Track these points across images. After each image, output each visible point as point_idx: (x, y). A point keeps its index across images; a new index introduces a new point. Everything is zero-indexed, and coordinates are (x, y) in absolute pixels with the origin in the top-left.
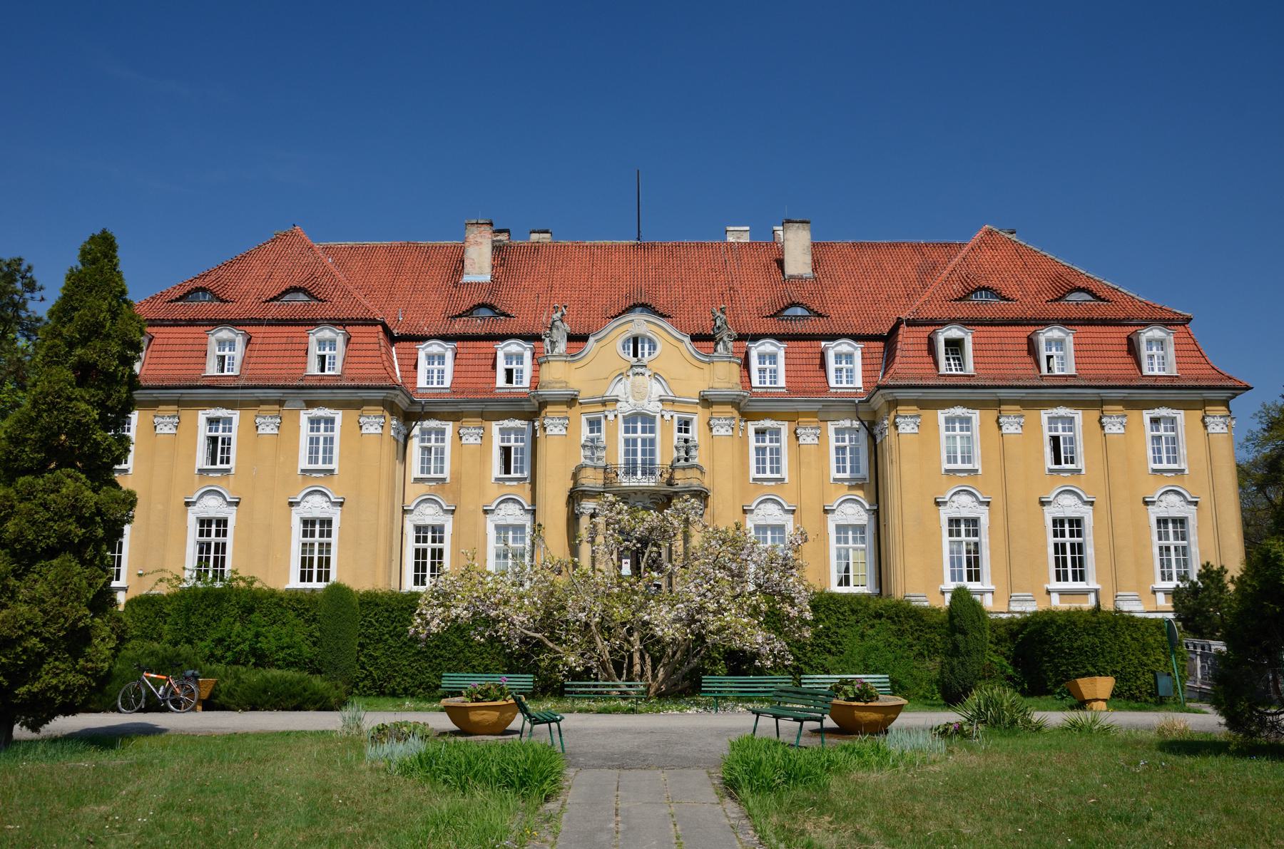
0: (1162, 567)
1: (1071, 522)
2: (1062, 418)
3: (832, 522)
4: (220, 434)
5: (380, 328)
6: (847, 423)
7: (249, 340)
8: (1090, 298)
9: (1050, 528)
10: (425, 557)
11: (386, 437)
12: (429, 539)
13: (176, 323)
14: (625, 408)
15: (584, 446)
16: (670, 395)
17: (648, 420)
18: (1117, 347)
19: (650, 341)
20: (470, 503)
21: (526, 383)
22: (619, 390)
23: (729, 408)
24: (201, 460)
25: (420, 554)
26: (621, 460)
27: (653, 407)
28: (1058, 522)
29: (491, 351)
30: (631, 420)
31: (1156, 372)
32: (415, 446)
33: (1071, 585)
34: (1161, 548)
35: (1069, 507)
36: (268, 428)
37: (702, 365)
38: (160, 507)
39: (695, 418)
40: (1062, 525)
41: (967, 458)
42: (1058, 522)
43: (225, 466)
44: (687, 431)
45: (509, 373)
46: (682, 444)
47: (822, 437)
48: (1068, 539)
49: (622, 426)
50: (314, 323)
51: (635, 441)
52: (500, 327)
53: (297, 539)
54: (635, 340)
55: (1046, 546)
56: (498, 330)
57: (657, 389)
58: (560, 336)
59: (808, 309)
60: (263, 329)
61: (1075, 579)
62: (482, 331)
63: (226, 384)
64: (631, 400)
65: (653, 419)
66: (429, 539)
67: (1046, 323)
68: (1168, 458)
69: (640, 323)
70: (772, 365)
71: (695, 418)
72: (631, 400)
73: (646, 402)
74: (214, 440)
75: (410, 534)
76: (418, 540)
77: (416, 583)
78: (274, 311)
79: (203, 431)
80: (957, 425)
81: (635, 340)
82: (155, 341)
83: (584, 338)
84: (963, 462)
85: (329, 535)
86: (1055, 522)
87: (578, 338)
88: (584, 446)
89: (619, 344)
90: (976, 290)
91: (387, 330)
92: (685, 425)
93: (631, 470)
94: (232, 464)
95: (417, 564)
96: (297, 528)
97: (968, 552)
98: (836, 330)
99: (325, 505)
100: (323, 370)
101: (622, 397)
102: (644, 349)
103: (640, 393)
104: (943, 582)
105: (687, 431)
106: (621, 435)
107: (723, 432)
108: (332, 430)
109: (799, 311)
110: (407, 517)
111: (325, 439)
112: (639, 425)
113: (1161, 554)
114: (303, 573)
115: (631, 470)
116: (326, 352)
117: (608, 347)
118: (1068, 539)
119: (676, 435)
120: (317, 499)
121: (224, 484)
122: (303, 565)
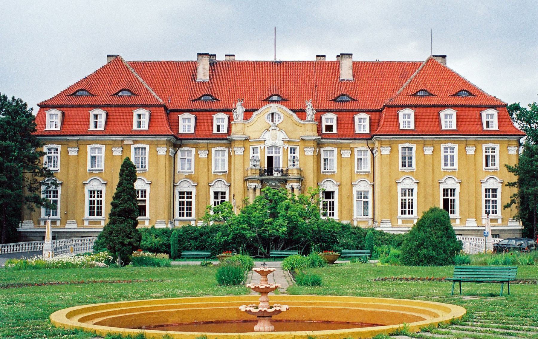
0: (486, 208)
1: (188, 193)
2: (142, 148)
3: (400, 187)
5: (163, 108)
6: (363, 149)
9: (442, 193)
10: (94, 204)
11: (168, 156)
12: (185, 197)
13: (73, 106)
14: (268, 144)
15: (251, 160)
16: (287, 138)
19: (279, 115)
20: (203, 182)
21: (225, 131)
22: (267, 136)
25: (182, 204)
27: (280, 144)
28: (487, 190)
33: (407, 216)
34: (486, 201)
35: (450, 184)
36: (73, 152)
38: (72, 186)
39: (298, 147)
40: (94, 193)
41: (145, 167)
42: (487, 190)
44: (294, 153)
46: (292, 159)
47: (209, 154)
48: (491, 198)
52: (214, 106)
53: (87, 199)
54: (273, 114)
55: (439, 201)
56: (213, 107)
57: (282, 136)
59: (350, 98)
60: (113, 109)
61: (409, 214)
63: (99, 134)
66: (185, 197)
67: (445, 107)
68: (451, 164)
69: (273, 107)
72: (271, 141)
73: (277, 141)
75: (177, 195)
76: (180, 198)
78: (116, 101)
80: (449, 150)
81: (273, 114)
84: (451, 166)
85: (57, 197)
86: (444, 190)
87: (249, 112)
88: (251, 160)
89: (266, 116)
90: (420, 91)
91: (166, 109)
92: (293, 150)
95: (412, 208)
97: (409, 203)
98: (361, 108)
99: (143, 184)
100: (96, 127)
101: (267, 139)
102: (276, 117)
103: (275, 138)
104: (40, 216)
105: (294, 153)
108: (453, 152)
110: (483, 185)
111: (451, 156)
113: (486, 203)
114: (90, 213)
117: (260, 117)
118: (491, 198)
119: (289, 154)
120: (491, 181)
122: (90, 209)
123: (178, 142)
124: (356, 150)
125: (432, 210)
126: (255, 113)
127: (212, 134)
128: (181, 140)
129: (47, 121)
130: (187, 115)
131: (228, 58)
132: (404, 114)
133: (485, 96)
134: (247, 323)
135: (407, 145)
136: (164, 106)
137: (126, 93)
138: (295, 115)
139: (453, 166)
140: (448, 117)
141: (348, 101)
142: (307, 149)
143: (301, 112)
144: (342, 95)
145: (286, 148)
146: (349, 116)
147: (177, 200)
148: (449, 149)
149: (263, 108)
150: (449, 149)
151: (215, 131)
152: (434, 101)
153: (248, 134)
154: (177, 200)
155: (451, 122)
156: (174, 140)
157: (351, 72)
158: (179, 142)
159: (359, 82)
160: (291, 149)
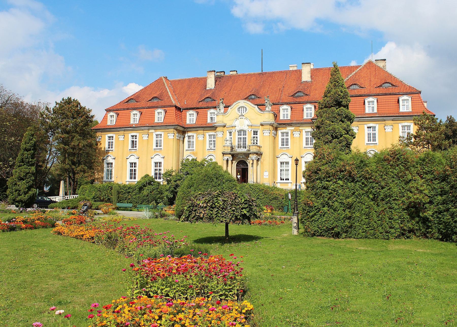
2: (407, 126)
4: (134, 140)
7: (166, 112)
8: (391, 85)
11: (175, 139)
14: (238, 128)
16: (250, 124)
17: (245, 131)
18: (394, 103)
19: (246, 108)
22: (237, 123)
23: (268, 127)
24: (154, 147)
26: (236, 144)
27: (246, 128)
28: (156, 163)
29: (302, 107)
30: (240, 132)
31: (406, 111)
32: (186, 139)
37: (261, 114)
39: (259, 130)
43: (287, 147)
45: (212, 118)
49: (237, 133)
50: (157, 107)
51: (241, 138)
52: (396, 90)
57: (247, 122)
58: (222, 106)
59: (392, 84)
62: (205, 106)
64: (239, 126)
65: (246, 131)
67: (369, 96)
68: (373, 140)
69: (242, 103)
70: (285, 112)
71: (259, 130)
74: (133, 141)
77: (131, 178)
78: (149, 104)
79: (130, 139)
82: (119, 115)
83: (228, 107)
84: (373, 141)
87: (227, 107)
91: (178, 109)
92: (255, 133)
93: (239, 146)
94: (137, 148)
96: (153, 165)
106: (237, 137)
107: (267, 134)
109: (253, 97)
110: (303, 158)
112: (242, 133)
115: (239, 146)
116: (159, 116)
117: (233, 110)
120: (284, 156)
121: (135, 153)
123: (183, 130)
124: (304, 131)
125: (147, 176)
126: (230, 108)
127: (399, 113)
128: (188, 128)
129: (108, 119)
130: (191, 112)
131: (231, 73)
132: (210, 113)
133: (405, 85)
134: (13, 233)
135: (110, 135)
136: (176, 107)
137: (354, 87)
138: (256, 107)
139: (375, 141)
140: (371, 103)
141: (302, 96)
142: (387, 127)
143: (261, 106)
144: (298, 92)
145: (250, 131)
146: (300, 107)
147: (279, 168)
148: (406, 127)
149: (235, 104)
150: (406, 127)
151: (209, 121)
152: (362, 92)
153: (225, 122)
154: (279, 168)
155: (373, 108)
156: (182, 129)
157: (309, 75)
158: (185, 130)
159: (315, 83)
160: (254, 132)
